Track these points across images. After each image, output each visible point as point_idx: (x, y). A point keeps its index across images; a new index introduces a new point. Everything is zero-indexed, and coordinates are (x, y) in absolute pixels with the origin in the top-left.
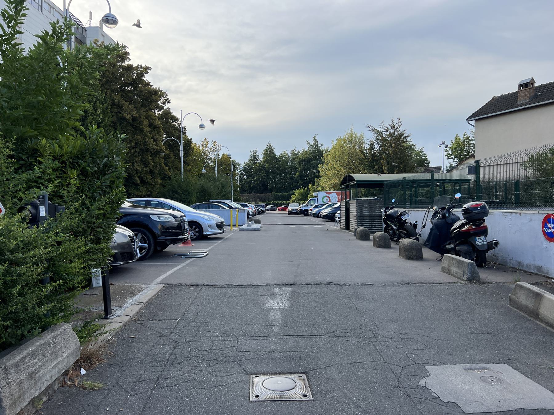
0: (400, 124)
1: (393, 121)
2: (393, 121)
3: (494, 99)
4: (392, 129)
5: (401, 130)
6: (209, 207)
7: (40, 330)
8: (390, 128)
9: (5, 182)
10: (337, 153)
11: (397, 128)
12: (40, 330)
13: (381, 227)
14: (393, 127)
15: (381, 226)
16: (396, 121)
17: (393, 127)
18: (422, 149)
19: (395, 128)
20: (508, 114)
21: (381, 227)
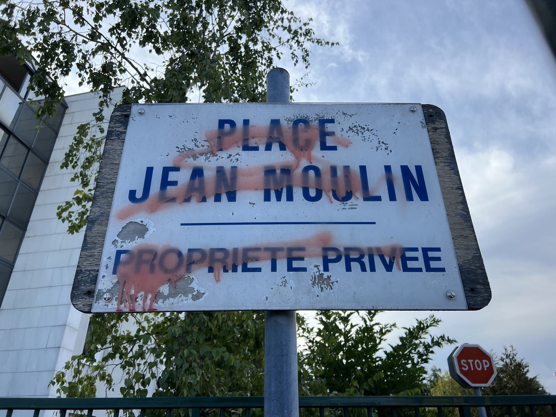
0: (515, 352)
1: (506, 349)
2: (506, 349)
3: (340, 261)
4: (507, 358)
5: (518, 359)
6: (184, 393)
7: (174, 92)
8: (504, 357)
9: (485, 393)
10: (447, 388)
11: (513, 357)
12: (174, 92)
13: (100, 253)
14: (508, 356)
15: (101, 252)
16: (509, 349)
17: (508, 356)
18: (113, 390)
19: (511, 357)
20: (5, 142)
21: (100, 253)
